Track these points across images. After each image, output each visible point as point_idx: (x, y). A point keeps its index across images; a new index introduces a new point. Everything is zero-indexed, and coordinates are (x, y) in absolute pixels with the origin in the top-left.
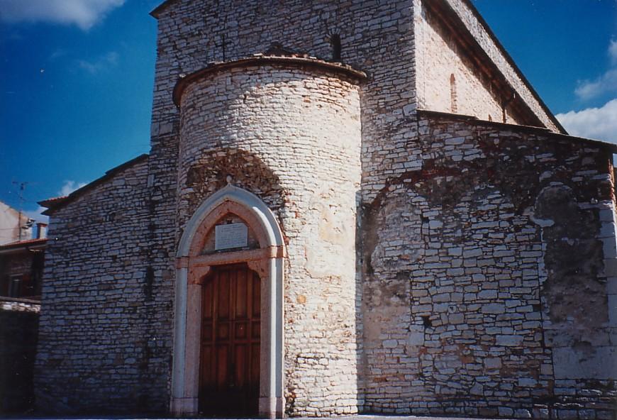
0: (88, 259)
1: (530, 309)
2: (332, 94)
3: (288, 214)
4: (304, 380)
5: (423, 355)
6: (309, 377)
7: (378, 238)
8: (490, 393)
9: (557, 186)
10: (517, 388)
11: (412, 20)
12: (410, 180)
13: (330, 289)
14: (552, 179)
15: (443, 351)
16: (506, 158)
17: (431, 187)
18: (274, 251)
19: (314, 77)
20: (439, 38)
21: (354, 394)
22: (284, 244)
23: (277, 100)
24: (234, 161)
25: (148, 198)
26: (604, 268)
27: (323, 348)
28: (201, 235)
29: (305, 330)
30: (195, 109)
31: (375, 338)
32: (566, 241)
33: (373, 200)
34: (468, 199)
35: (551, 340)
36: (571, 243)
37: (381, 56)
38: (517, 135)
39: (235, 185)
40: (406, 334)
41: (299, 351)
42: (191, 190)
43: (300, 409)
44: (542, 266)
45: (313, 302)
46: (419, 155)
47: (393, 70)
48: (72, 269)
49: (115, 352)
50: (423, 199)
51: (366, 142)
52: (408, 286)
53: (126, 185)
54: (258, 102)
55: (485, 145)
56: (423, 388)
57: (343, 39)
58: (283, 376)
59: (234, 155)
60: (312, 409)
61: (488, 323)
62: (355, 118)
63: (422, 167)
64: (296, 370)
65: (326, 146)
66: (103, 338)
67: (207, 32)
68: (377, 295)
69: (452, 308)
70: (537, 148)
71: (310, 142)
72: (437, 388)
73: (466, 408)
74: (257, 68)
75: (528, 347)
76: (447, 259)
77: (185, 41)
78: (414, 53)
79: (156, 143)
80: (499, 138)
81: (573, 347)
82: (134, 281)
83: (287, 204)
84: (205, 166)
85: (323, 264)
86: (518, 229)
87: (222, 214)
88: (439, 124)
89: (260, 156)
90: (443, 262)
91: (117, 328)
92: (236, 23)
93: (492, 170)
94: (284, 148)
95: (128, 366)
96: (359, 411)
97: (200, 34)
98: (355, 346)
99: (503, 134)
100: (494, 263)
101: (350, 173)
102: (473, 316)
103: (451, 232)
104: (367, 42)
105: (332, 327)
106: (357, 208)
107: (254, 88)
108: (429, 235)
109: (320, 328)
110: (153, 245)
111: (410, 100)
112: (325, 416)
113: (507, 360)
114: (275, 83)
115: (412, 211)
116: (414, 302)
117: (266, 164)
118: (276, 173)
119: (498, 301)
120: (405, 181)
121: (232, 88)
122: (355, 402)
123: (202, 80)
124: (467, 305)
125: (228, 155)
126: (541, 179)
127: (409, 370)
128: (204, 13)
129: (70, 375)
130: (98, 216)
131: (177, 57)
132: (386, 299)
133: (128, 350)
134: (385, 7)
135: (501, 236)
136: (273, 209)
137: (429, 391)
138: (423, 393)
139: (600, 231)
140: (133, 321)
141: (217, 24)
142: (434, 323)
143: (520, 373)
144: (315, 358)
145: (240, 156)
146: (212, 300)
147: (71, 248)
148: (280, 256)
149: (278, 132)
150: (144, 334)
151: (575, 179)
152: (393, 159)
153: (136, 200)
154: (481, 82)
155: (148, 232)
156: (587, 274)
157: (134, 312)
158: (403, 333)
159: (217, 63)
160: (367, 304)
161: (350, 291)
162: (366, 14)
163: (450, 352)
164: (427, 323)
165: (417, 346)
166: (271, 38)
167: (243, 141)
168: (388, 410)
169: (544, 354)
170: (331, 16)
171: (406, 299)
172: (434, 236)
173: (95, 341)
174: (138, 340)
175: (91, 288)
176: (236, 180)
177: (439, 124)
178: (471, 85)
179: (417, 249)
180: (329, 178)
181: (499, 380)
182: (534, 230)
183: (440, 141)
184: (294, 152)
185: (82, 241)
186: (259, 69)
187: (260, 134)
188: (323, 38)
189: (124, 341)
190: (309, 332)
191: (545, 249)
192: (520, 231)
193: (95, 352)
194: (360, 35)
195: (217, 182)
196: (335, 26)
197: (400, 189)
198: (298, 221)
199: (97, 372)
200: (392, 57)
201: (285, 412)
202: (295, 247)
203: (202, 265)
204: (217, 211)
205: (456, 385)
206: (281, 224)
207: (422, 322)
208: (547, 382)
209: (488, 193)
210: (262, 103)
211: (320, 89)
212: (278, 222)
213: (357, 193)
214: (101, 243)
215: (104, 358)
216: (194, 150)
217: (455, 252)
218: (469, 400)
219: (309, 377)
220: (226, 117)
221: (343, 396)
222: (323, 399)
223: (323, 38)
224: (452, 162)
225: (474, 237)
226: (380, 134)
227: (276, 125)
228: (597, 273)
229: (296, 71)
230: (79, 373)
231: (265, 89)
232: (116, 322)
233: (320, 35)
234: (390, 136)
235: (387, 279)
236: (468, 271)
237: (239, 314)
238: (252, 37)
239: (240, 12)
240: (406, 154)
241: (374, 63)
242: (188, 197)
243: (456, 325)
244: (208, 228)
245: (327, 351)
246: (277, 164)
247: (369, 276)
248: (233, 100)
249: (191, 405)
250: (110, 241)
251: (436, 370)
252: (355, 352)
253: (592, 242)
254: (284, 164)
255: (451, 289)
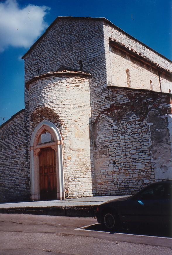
0: (8, 148)
1: (147, 156)
2: (77, 83)
3: (63, 129)
4: (71, 186)
5: (113, 174)
6: (73, 185)
7: (97, 134)
8: (135, 186)
9: (154, 110)
10: (143, 184)
11: (104, 53)
12: (106, 112)
13: (80, 154)
14: (152, 108)
15: (120, 172)
16: (137, 101)
17: (113, 114)
18: (59, 143)
19: (70, 78)
20: (119, 57)
21: (91, 189)
22: (62, 140)
23: (57, 88)
24: (45, 111)
25: (25, 125)
26: (170, 139)
27: (78, 174)
28: (37, 138)
29: (71, 169)
30: (31, 94)
31: (98, 169)
32: (157, 131)
33: (95, 120)
34: (126, 117)
35: (154, 166)
36: (159, 131)
37: (95, 67)
38: (140, 93)
39: (46, 120)
40: (108, 167)
41: (69, 176)
42: (32, 123)
43: (70, 196)
44: (150, 140)
45: (73, 159)
46: (109, 102)
47: (99, 72)
48: (3, 152)
49: (18, 180)
50: (111, 119)
51: (92, 99)
52: (108, 150)
53: (18, 121)
54: (50, 89)
55: (130, 97)
56: (114, 186)
57: (83, 62)
58: (64, 185)
59: (44, 109)
60: (75, 196)
61: (133, 161)
62: (88, 91)
63: (110, 107)
64: (68, 183)
65: (76, 103)
66: (14, 175)
67: (40, 63)
68: (98, 154)
69: (122, 157)
70: (147, 97)
71: (70, 102)
72: (118, 186)
73: (128, 192)
74: (49, 77)
75: (147, 169)
76: (119, 140)
77: (33, 67)
78: (106, 65)
79: (26, 105)
80: (134, 94)
81: (161, 168)
82: (23, 155)
83: (62, 125)
84: (36, 114)
85: (77, 145)
86: (142, 127)
87: (43, 130)
88: (115, 90)
89: (52, 109)
90: (118, 141)
91: (18, 171)
92: (49, 59)
93: (133, 106)
94: (60, 105)
95: (22, 184)
96: (93, 195)
97: (38, 64)
98: (91, 173)
99: (136, 92)
100: (134, 140)
101: (86, 111)
102: (128, 159)
103: (120, 130)
104: (91, 62)
105: (81, 166)
106: (90, 124)
107: (49, 84)
108: (114, 132)
109: (77, 167)
110: (27, 142)
111: (105, 83)
112: (79, 198)
113: (140, 174)
114: (56, 82)
115: (108, 123)
116: (110, 156)
117: (54, 111)
118: (58, 114)
119: (136, 154)
120: (105, 112)
121: (42, 85)
122: (92, 192)
123: (33, 83)
124: (126, 156)
125: (42, 109)
126: (148, 108)
127: (109, 180)
128: (39, 57)
129: (5, 188)
130: (10, 133)
131: (31, 73)
132: (101, 156)
133: (22, 179)
134: (96, 49)
135: (136, 130)
136: (58, 127)
137: (116, 187)
138: (114, 188)
139: (168, 126)
140: (23, 169)
141: (43, 60)
142: (116, 163)
143: (144, 179)
144: (75, 178)
145: (46, 109)
146: (42, 161)
147: (3, 145)
148: (61, 144)
149: (58, 99)
150: (27, 173)
151: (159, 107)
152: (101, 105)
153: (22, 126)
154: (145, 68)
155: (26, 137)
156: (165, 142)
157: (23, 166)
158: (106, 167)
159: (36, 77)
160: (95, 158)
161: (88, 154)
162: (90, 52)
163: (122, 173)
164: (114, 163)
165: (111, 171)
166: (60, 63)
167: (46, 104)
168: (103, 194)
169: (152, 171)
170: (79, 54)
171: (107, 155)
172: (115, 132)
173: (12, 176)
174: (25, 175)
175: (9, 158)
176: (46, 118)
177: (115, 90)
178: (139, 71)
179: (110, 137)
180: (77, 114)
181: (138, 181)
182: (147, 127)
183: (116, 97)
184: (64, 106)
185: (6, 142)
186: (50, 77)
187: (52, 101)
188: (77, 62)
189: (21, 176)
190: (73, 169)
191: (151, 134)
192: (143, 128)
193: (12, 180)
194: (88, 60)
195: (40, 119)
196: (80, 58)
197: (103, 116)
198: (66, 131)
199: (13, 187)
200: (99, 67)
201: (65, 197)
202: (66, 140)
203: (38, 149)
204: (41, 129)
205: (124, 184)
206: (61, 132)
207: (113, 163)
208: (153, 181)
209: (132, 115)
210: (52, 89)
211: (73, 82)
212: (59, 132)
213: (89, 118)
214: (11, 142)
215: (15, 182)
216: (32, 108)
217: (122, 137)
218: (128, 189)
219: (73, 185)
220: (40, 96)
221: (86, 191)
222: (78, 192)
223: (77, 62)
224: (120, 104)
225: (128, 131)
226: (96, 96)
227: (57, 97)
228: (168, 141)
229: (63, 77)
230: (8, 187)
231: (52, 84)
232: (18, 169)
233: (76, 61)
234: (100, 96)
235: (101, 148)
236: (126, 144)
237: (50, 164)
238: (54, 64)
239: (50, 55)
240: (105, 102)
241: (93, 70)
242: (32, 125)
243: (123, 163)
244: (39, 135)
245: (80, 175)
246: (58, 111)
247: (95, 148)
248: (42, 89)
249: (37, 197)
250: (14, 141)
251: (118, 179)
252: (91, 175)
253: (165, 130)
254: (60, 111)
255: (121, 150)
